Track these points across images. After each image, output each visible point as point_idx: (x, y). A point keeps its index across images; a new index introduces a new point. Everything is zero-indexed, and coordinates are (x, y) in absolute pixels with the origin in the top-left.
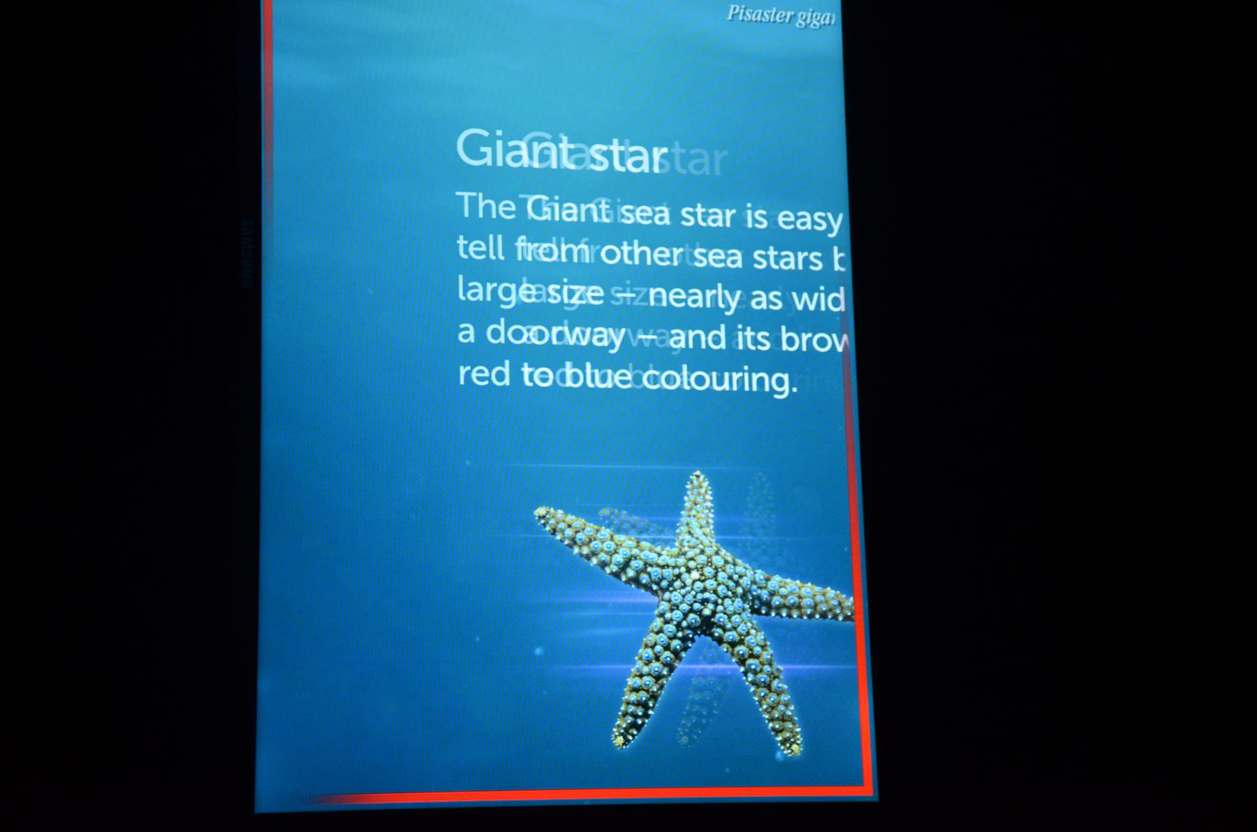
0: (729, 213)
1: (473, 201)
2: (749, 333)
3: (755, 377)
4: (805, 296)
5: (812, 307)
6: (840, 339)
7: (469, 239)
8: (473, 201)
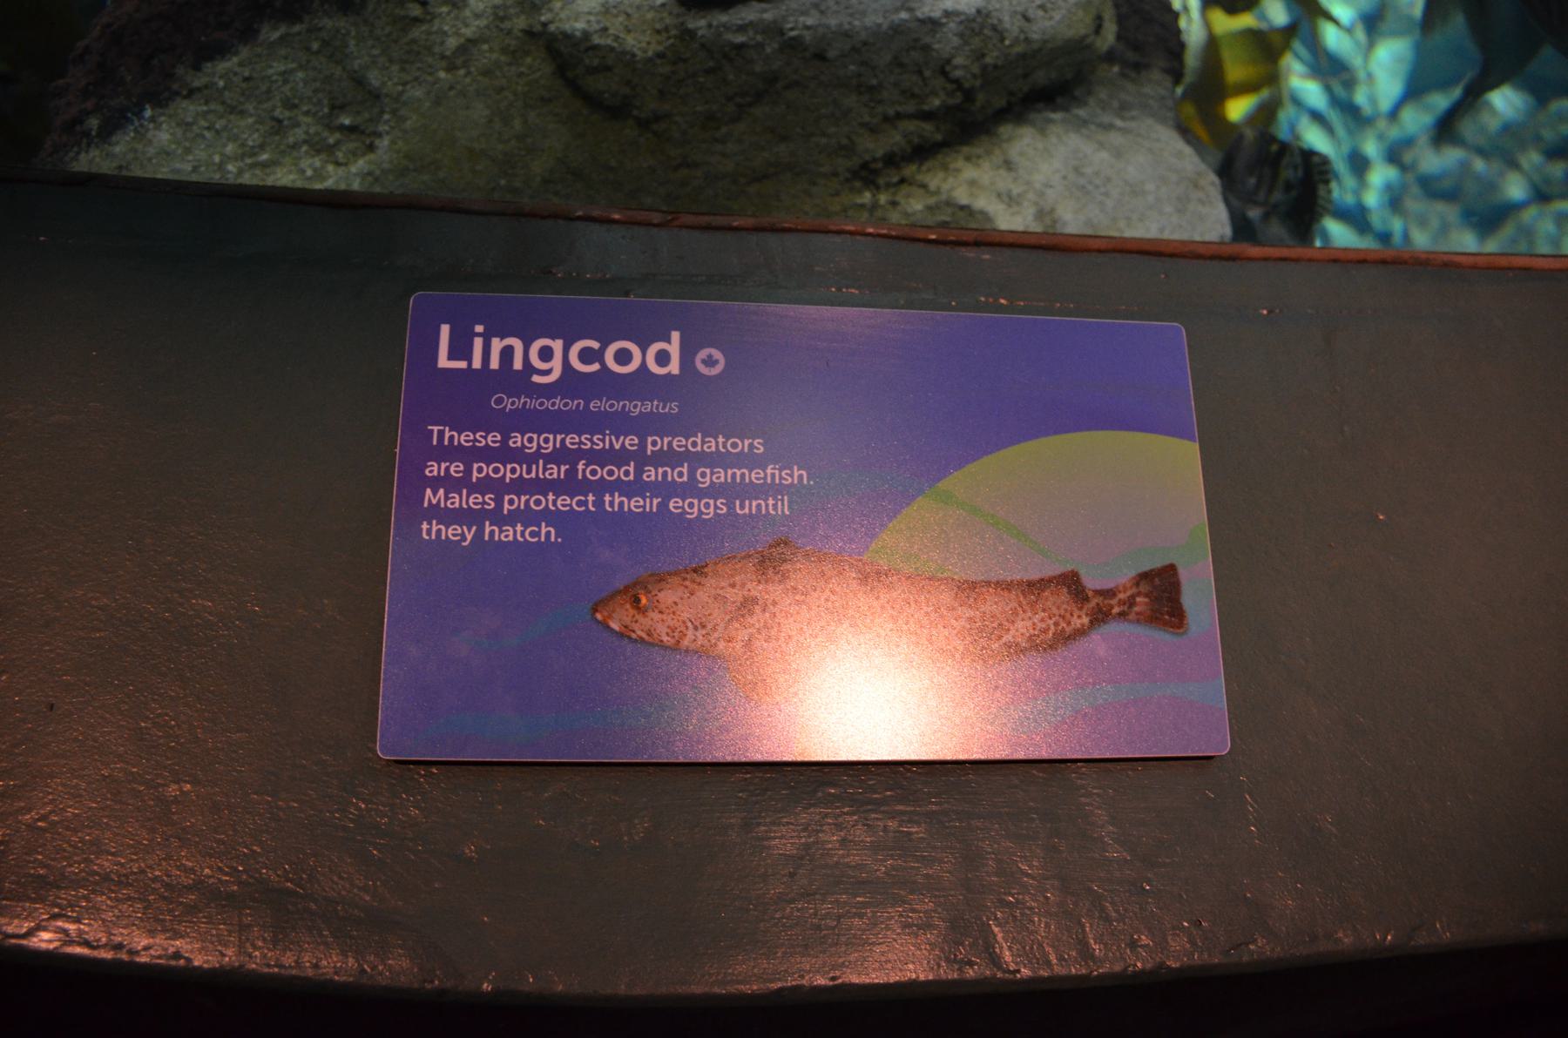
0: (563, 468)
1: (441, 433)
3: (497, 345)
7: (557, 495)
8: (441, 433)
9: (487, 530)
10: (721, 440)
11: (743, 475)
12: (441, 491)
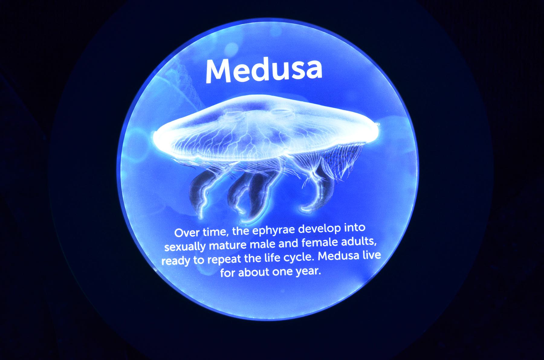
2: (366, 239)
3: (349, 227)
6: (187, 260)
11: (217, 232)
12: (325, 253)
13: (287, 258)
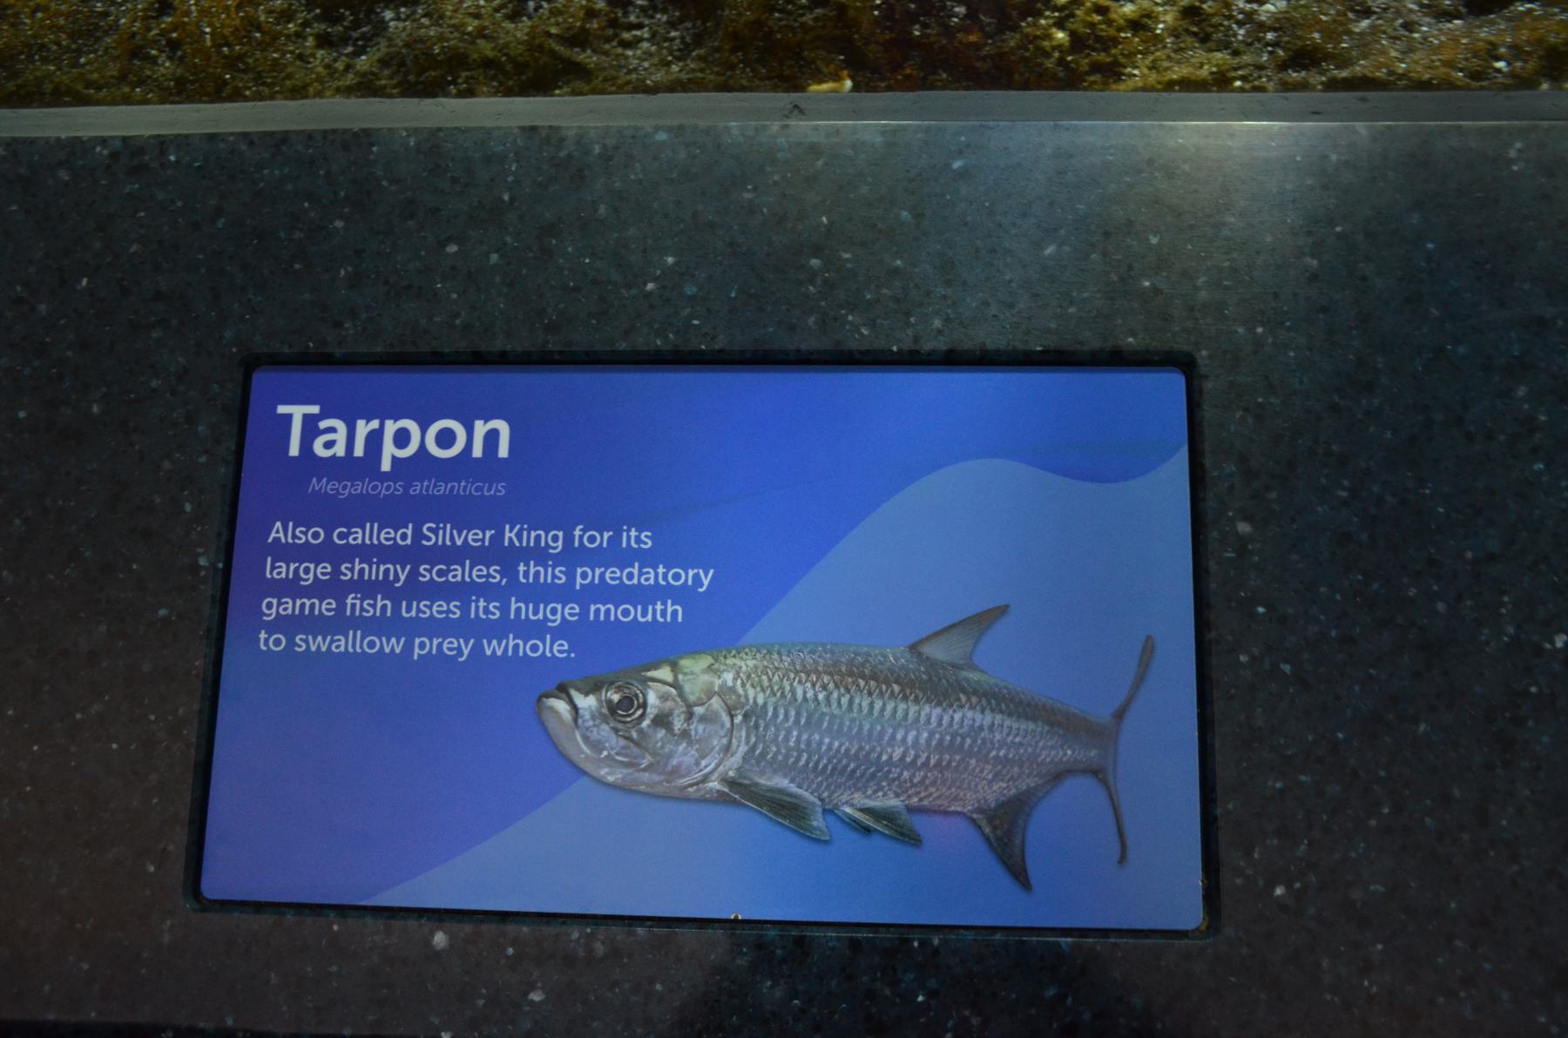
3: (533, 534)
4: (495, 642)
5: (499, 653)
9: (513, 607)
10: (661, 570)
11: (608, 612)
13: (341, 536)
